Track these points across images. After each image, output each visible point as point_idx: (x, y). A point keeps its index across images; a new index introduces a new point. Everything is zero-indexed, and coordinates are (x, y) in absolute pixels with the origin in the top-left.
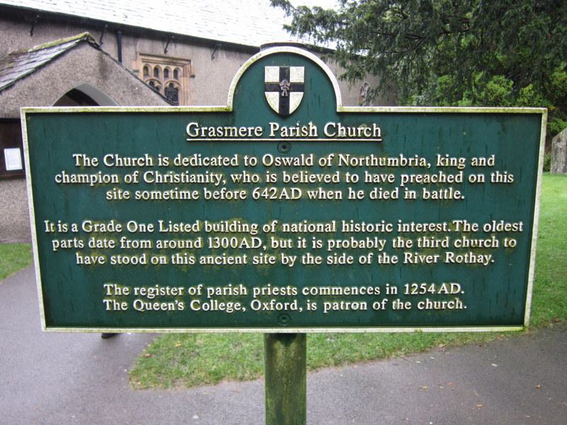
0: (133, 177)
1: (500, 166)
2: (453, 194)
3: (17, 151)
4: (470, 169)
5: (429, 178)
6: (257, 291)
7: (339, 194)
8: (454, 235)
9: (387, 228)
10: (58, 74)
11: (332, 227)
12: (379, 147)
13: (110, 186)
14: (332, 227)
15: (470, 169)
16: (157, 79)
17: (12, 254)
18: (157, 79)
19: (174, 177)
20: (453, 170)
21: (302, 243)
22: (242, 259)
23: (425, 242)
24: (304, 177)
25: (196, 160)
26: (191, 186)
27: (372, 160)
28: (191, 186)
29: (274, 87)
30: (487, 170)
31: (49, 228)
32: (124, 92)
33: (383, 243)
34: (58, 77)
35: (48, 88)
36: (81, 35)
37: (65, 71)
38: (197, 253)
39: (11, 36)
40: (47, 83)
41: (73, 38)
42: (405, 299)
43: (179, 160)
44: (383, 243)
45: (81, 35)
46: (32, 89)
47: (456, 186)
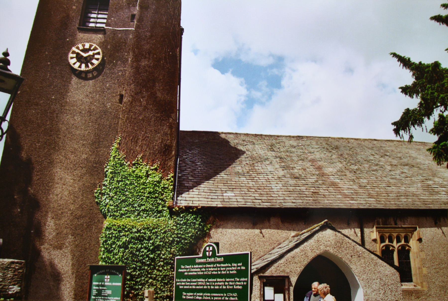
0: (188, 270)
1: (243, 266)
2: (235, 272)
3: (282, 295)
4: (238, 266)
5: (231, 269)
6: (204, 294)
7: (217, 273)
8: (235, 282)
9: (224, 280)
10: (308, 247)
11: (215, 280)
12: (224, 263)
13: (185, 272)
14: (215, 280)
15: (238, 266)
16: (391, 244)
17: (118, 243)
18: (391, 244)
19: (194, 270)
20: (234, 267)
21: (211, 284)
22: (202, 287)
23: (231, 283)
24: (212, 269)
25: (197, 266)
26: (195, 272)
27: (222, 265)
28: (195, 272)
29: (208, 251)
30: (240, 266)
31: (177, 281)
32: (352, 256)
33: (223, 283)
34: (309, 249)
35: (302, 256)
36: (323, 223)
37: (313, 245)
38: (196, 286)
39: (294, 226)
40: (302, 253)
41: (318, 225)
42: (227, 297)
43: (195, 266)
44: (223, 283)
45: (323, 223)
46: (293, 257)
47: (235, 270)
